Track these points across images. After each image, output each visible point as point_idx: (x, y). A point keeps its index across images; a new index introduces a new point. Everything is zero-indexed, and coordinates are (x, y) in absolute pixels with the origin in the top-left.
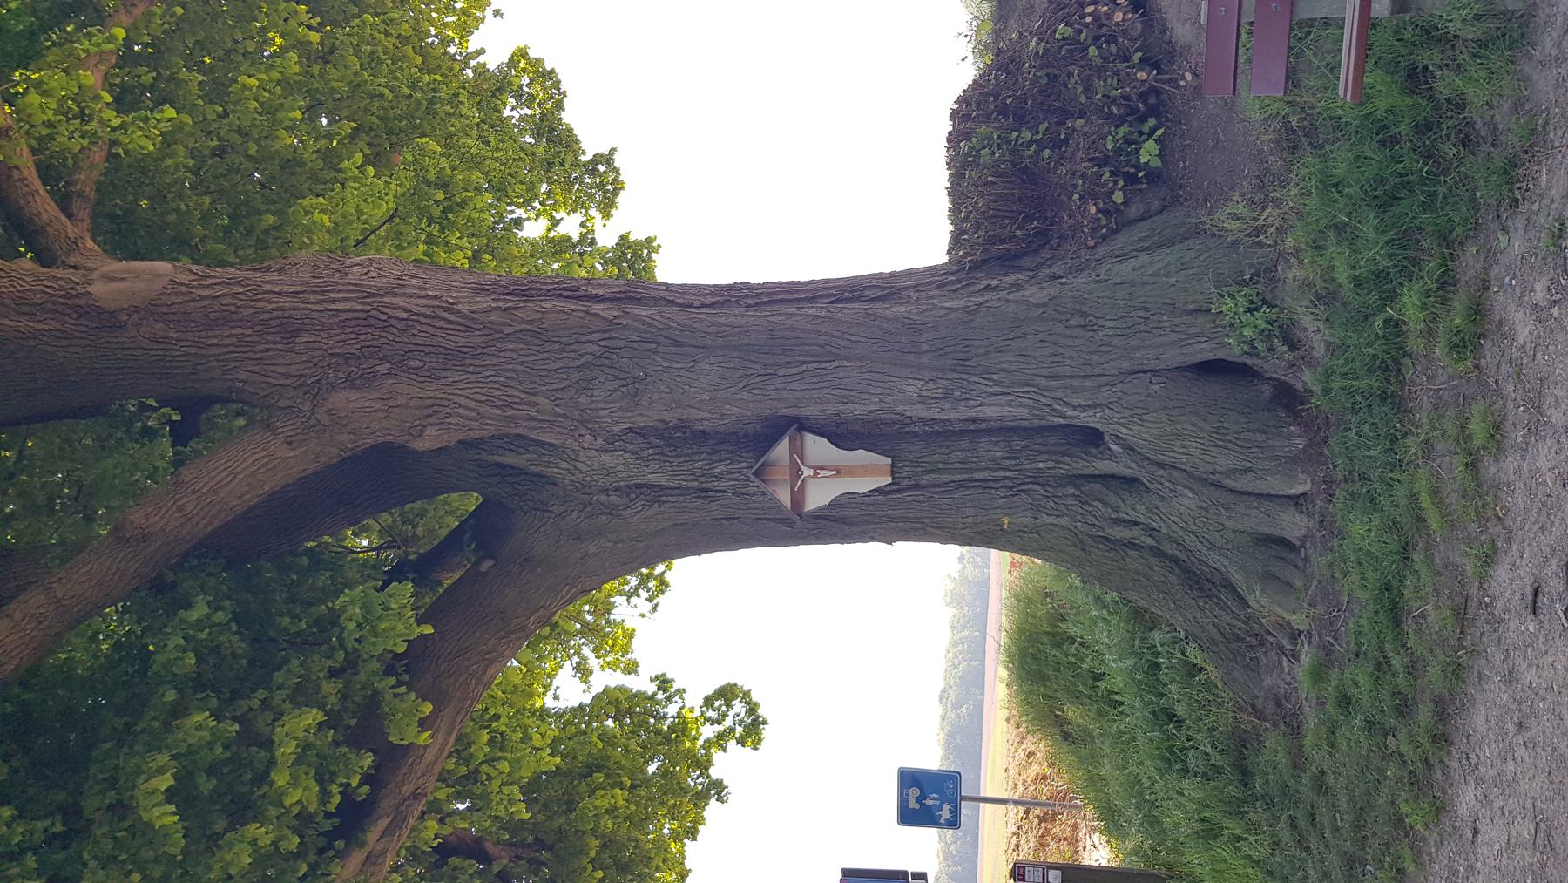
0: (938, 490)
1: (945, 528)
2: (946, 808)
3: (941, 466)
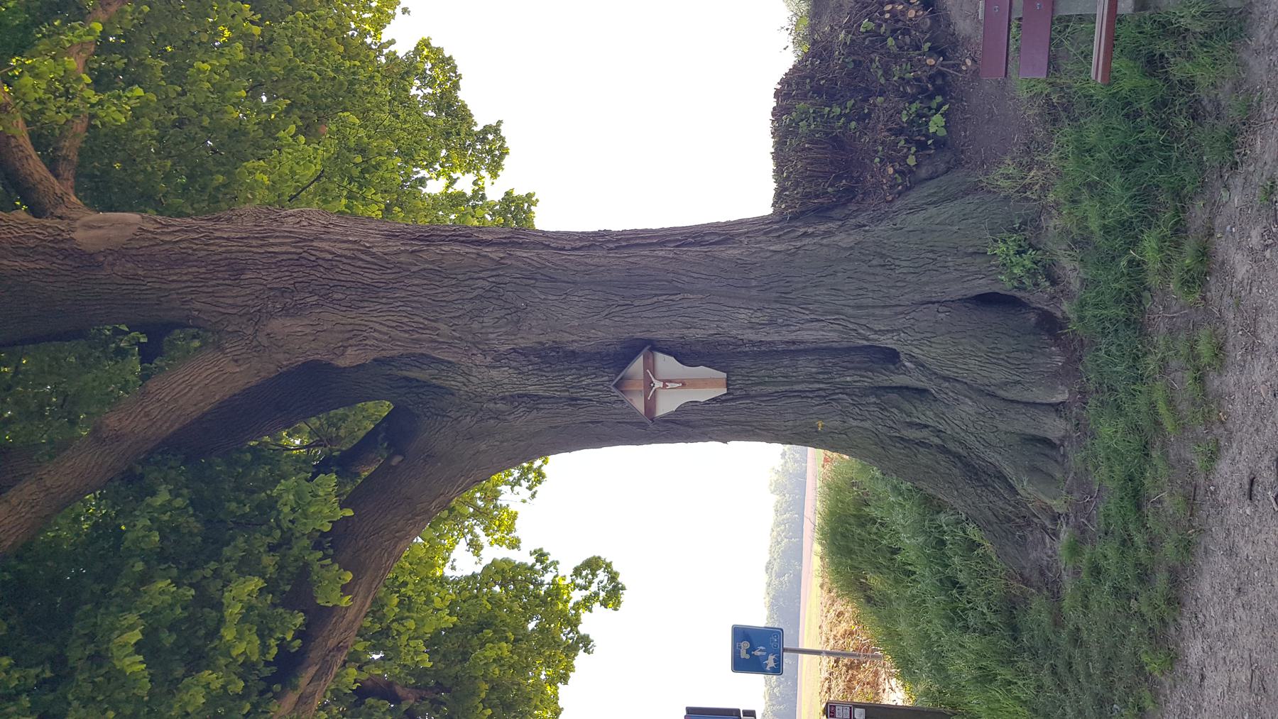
0: (765, 399)
1: (770, 430)
2: (771, 658)
3: (767, 379)
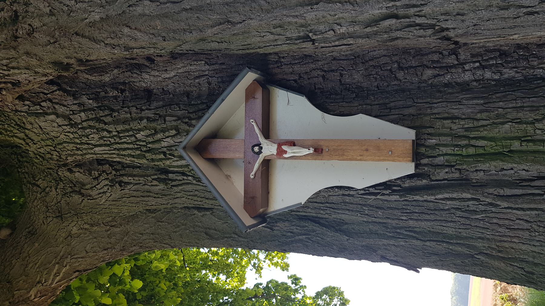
0: (508, 192)
1: (515, 259)
3: (516, 145)
